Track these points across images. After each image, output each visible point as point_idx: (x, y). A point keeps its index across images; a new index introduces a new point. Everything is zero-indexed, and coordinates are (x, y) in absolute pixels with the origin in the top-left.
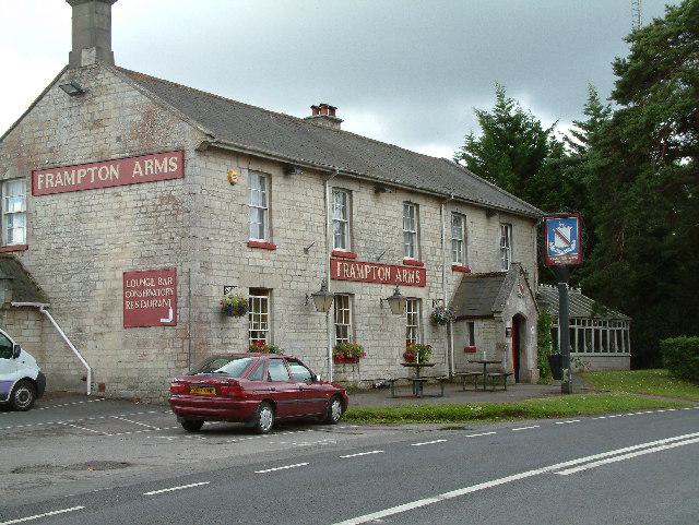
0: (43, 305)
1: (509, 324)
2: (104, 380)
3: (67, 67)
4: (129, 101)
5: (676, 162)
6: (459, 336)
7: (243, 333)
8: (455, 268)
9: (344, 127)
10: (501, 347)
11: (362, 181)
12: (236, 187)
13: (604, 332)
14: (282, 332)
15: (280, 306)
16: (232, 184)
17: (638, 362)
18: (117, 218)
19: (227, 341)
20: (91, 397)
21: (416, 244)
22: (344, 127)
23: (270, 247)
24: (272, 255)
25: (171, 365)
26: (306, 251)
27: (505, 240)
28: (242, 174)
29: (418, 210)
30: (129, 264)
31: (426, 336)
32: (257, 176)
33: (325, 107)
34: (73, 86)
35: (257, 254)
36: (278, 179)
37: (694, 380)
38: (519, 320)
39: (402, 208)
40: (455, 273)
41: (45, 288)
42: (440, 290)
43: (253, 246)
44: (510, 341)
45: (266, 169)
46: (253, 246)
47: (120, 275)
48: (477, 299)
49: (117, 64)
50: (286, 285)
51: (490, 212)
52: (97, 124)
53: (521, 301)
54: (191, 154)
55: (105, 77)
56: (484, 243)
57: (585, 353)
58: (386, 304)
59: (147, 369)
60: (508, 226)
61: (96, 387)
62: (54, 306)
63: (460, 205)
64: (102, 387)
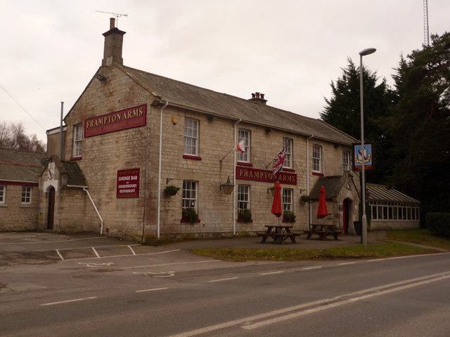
0: (84, 187)
1: (341, 204)
2: (109, 227)
3: (101, 67)
4: (124, 81)
5: (376, 86)
6: (313, 208)
7: (179, 204)
8: (314, 174)
9: (267, 104)
10: (337, 216)
11: (258, 126)
12: (177, 126)
13: (413, 210)
14: (203, 203)
15: (200, 190)
16: (174, 124)
17: (423, 225)
18: (117, 142)
19: (168, 208)
20: (103, 235)
21: (197, 146)
22: (267, 104)
23: (199, 159)
24: (199, 163)
25: (136, 220)
26: (221, 161)
27: (315, 154)
28: (181, 120)
29: (251, 133)
30: (121, 166)
31: (295, 208)
32: (193, 120)
33: (258, 94)
34: (102, 77)
35: (190, 162)
36: (204, 124)
37: (447, 237)
38: (348, 202)
39: (282, 140)
40: (314, 176)
41: (87, 178)
42: (306, 184)
43: (185, 157)
44: (341, 213)
45: (197, 117)
46: (185, 157)
47: (116, 171)
48: (325, 189)
49: (125, 64)
50: (207, 180)
51: (336, 145)
52: (111, 94)
53: (349, 191)
54: (149, 108)
55: (115, 71)
56: (332, 162)
57: (388, 220)
58: (270, 191)
59: (126, 222)
60: (288, 142)
61: (105, 229)
62: (90, 187)
63: (318, 142)
64: (107, 230)
